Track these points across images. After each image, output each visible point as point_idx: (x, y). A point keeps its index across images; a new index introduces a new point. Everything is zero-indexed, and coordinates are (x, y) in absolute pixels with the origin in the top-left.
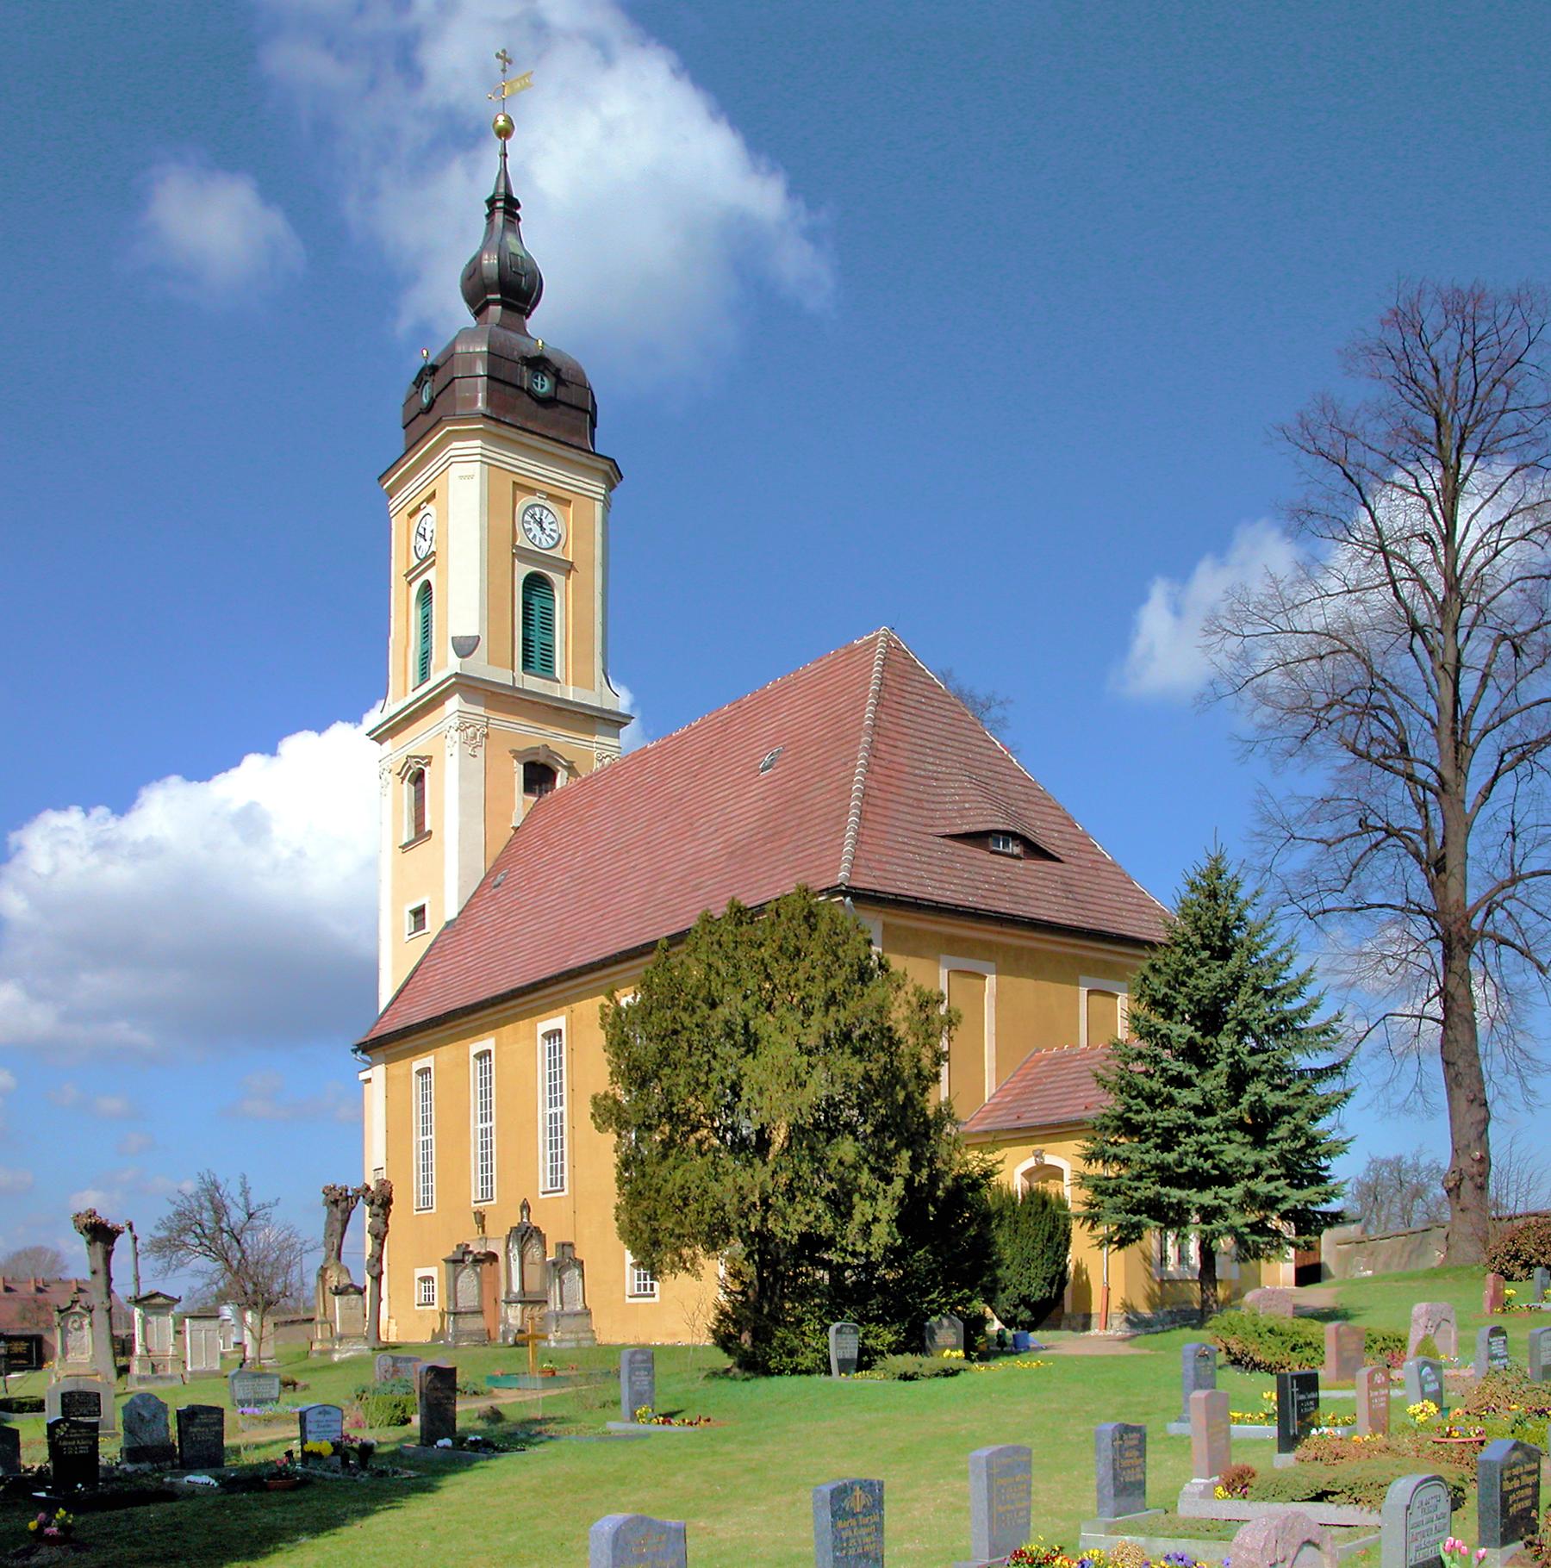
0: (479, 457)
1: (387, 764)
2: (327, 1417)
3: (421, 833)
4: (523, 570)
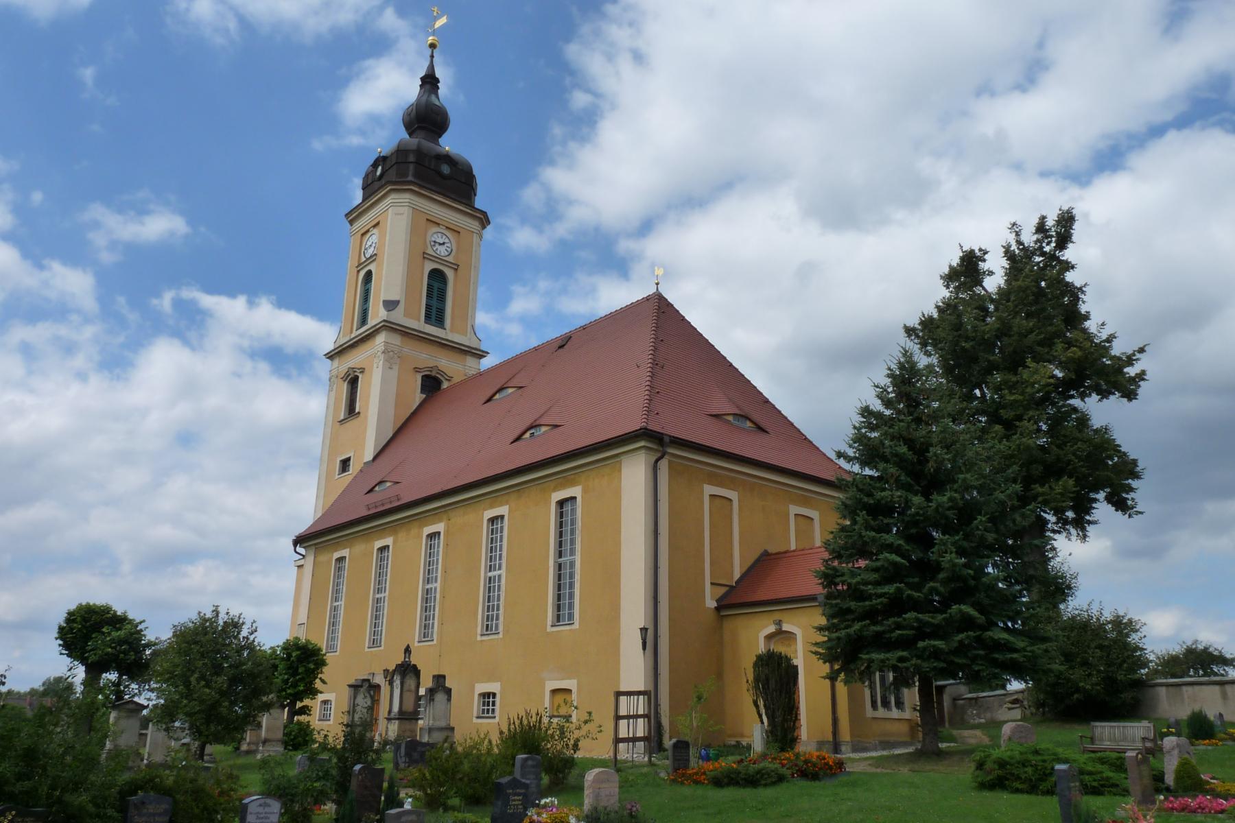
0: (407, 204)
1: (335, 372)
2: (267, 809)
3: (351, 410)
4: (429, 266)
